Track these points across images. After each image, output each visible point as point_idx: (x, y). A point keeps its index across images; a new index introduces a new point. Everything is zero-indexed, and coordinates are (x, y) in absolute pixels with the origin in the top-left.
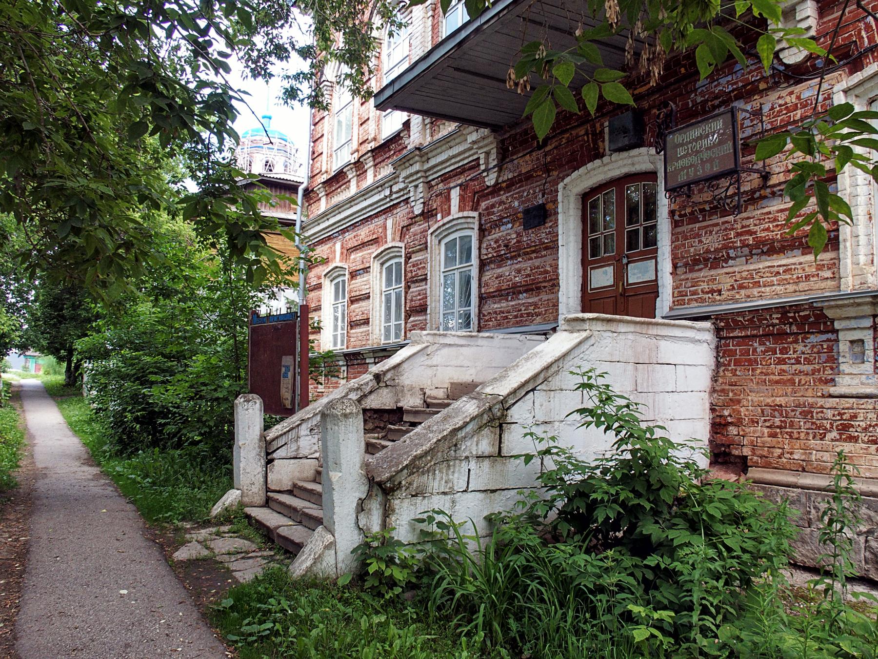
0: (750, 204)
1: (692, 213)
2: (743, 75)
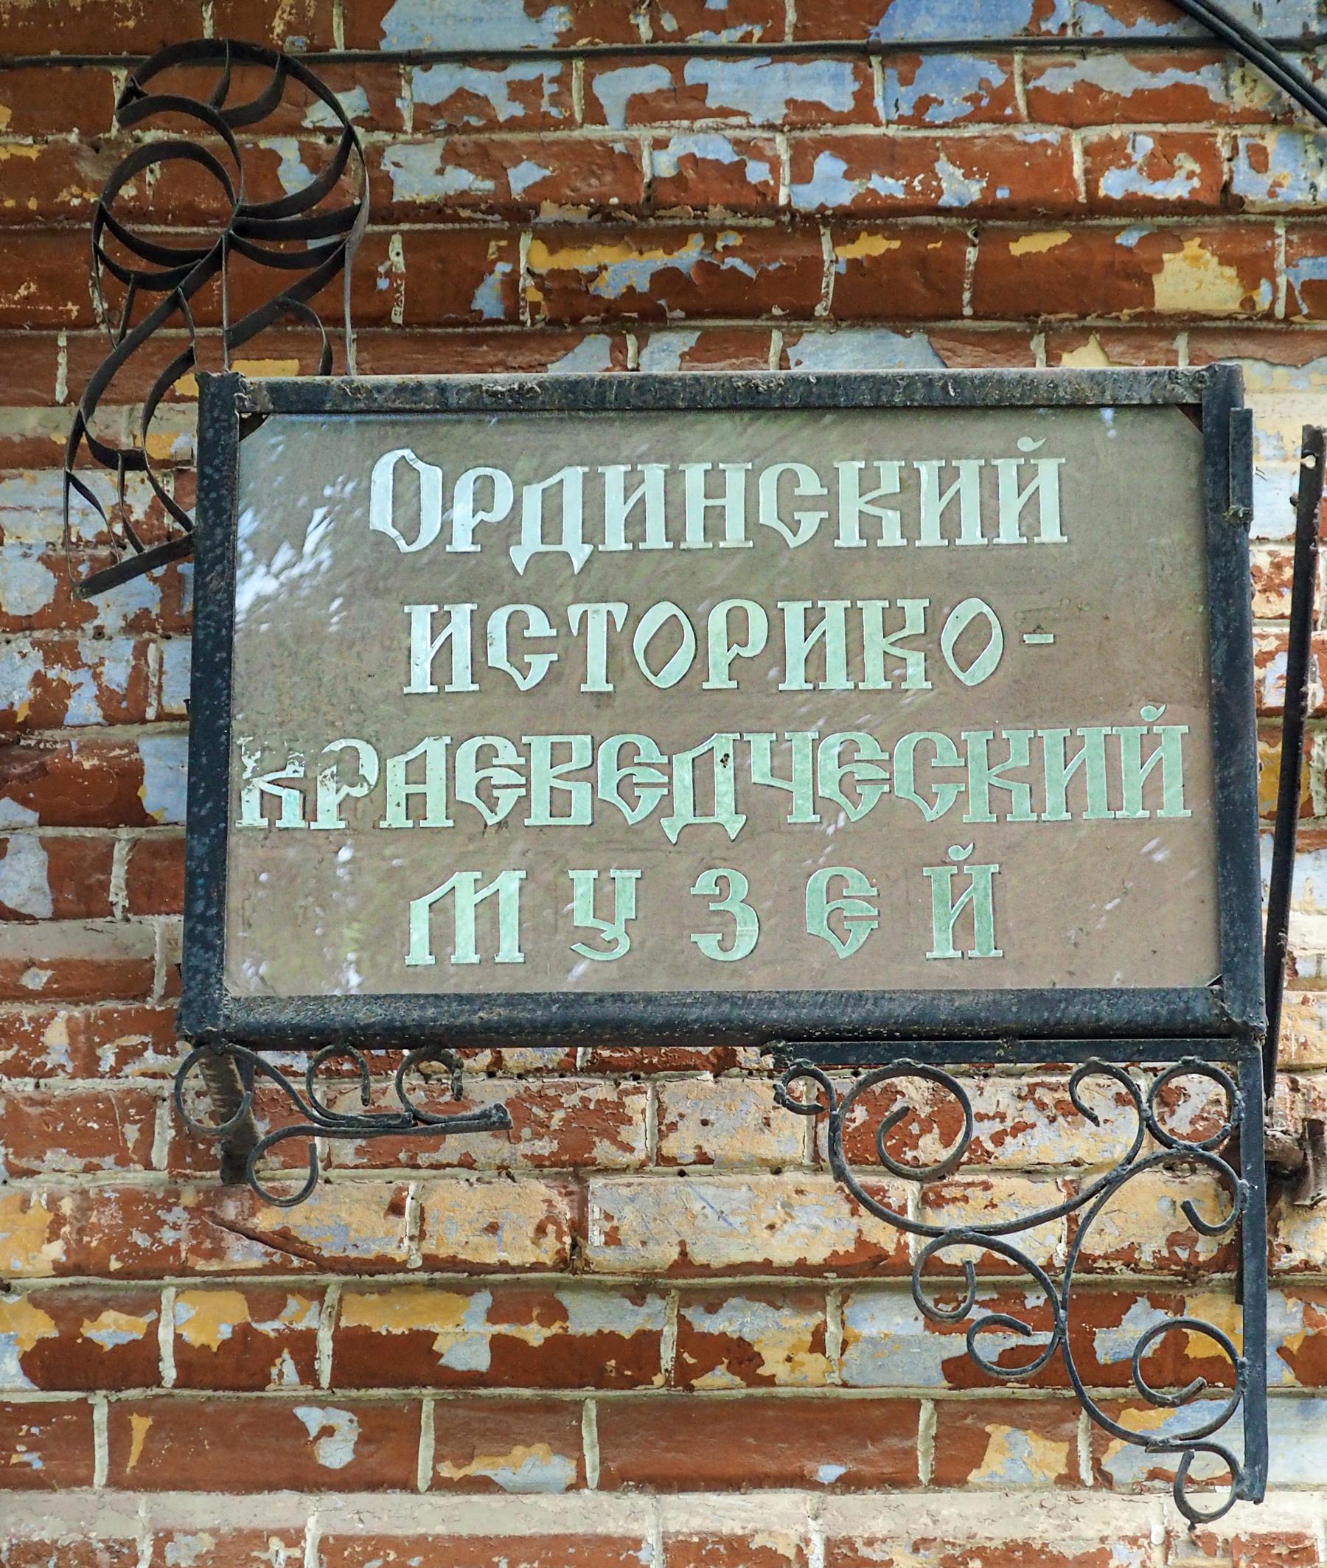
0: (1010, 1411)
1: (241, 1362)
2: (991, 107)
